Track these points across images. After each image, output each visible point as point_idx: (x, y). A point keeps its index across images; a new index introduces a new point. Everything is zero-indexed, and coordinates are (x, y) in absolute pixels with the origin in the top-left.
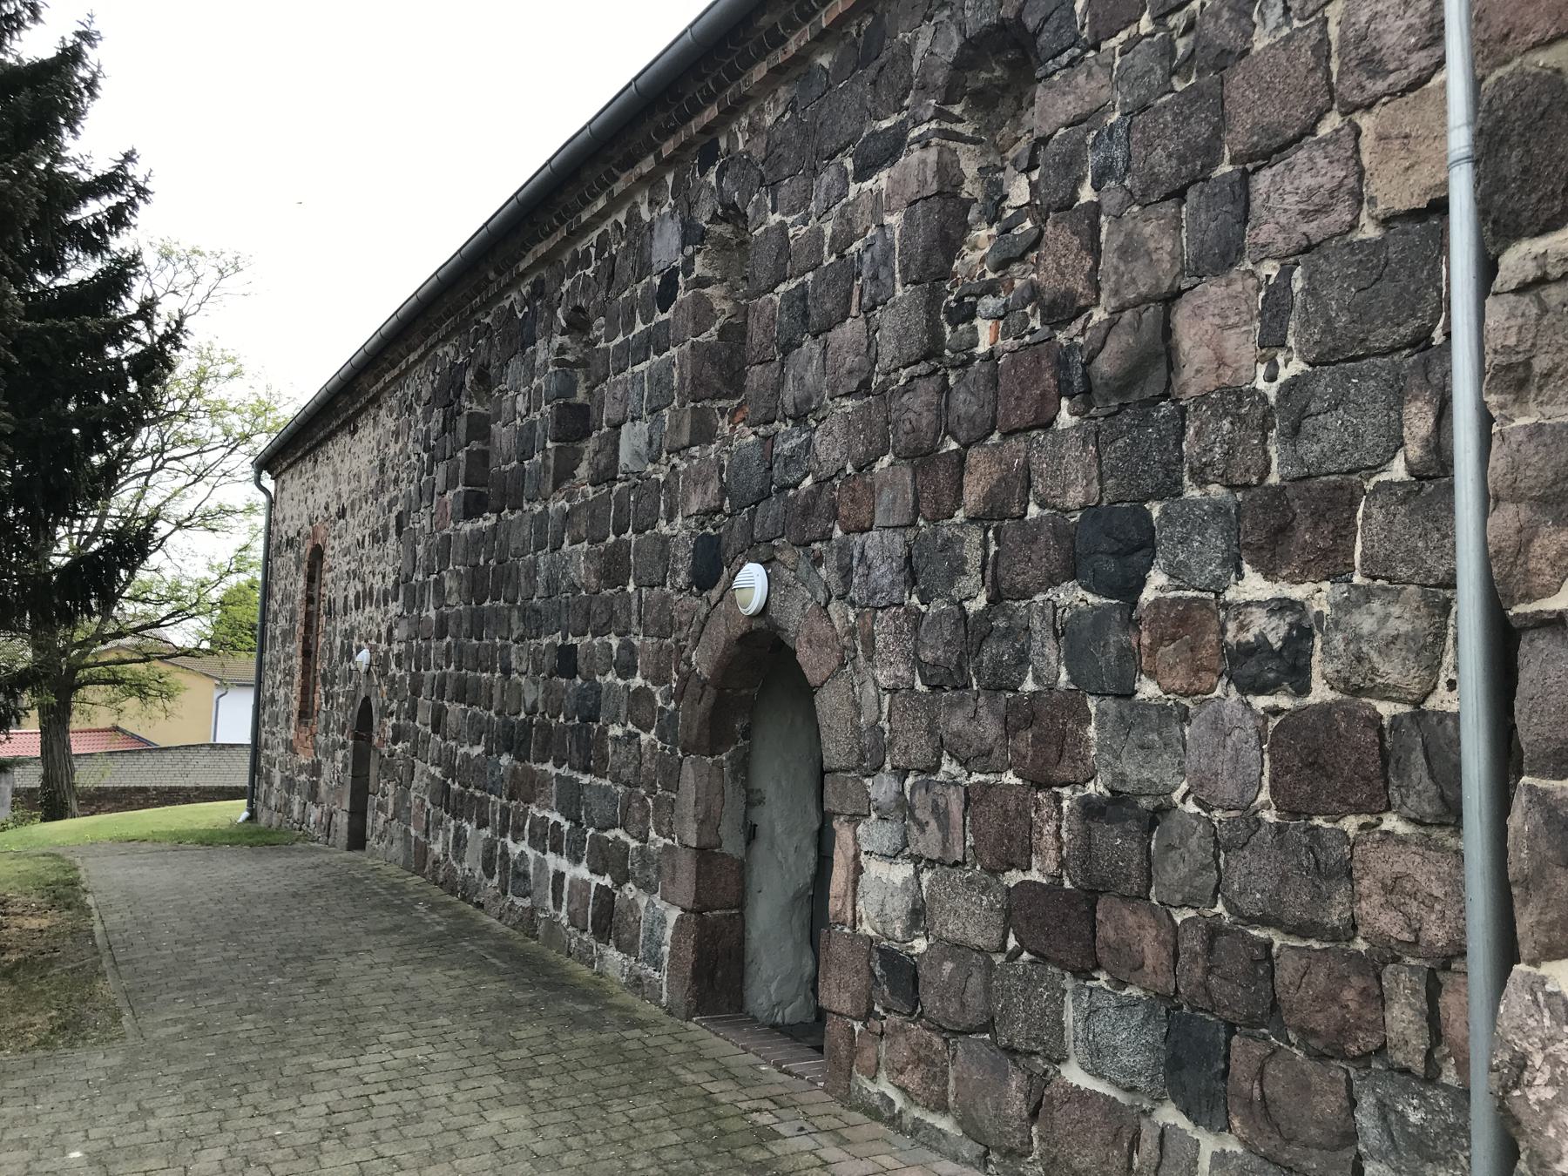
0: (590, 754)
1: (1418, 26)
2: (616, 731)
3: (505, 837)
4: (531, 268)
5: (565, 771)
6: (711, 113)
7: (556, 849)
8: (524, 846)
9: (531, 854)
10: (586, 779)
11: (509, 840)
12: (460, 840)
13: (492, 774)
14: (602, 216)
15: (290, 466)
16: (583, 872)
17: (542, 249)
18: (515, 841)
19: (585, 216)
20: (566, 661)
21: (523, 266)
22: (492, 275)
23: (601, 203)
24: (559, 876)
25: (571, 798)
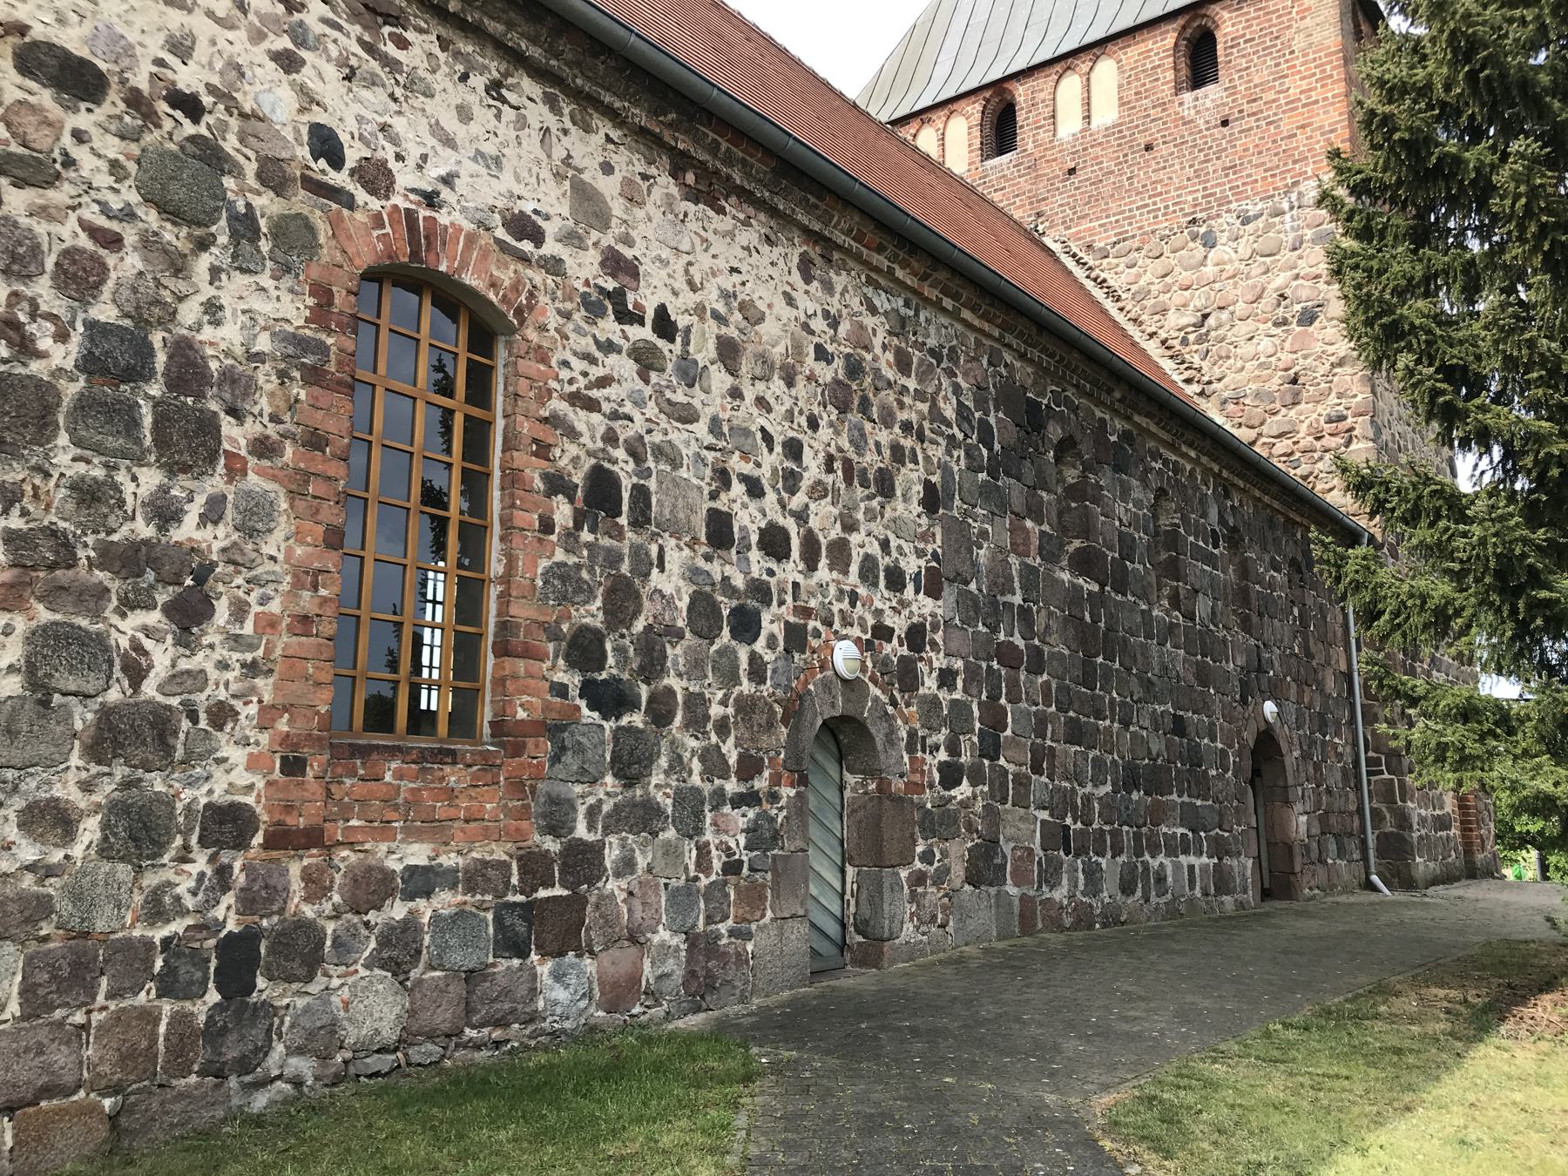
0: (1201, 786)
1: (208, 333)
2: (1214, 772)
3: (1023, 897)
4: (1138, 426)
5: (1185, 798)
6: (1241, 484)
7: (1186, 852)
8: (1161, 858)
9: (1167, 862)
10: (1199, 803)
11: (1147, 857)
12: (1093, 873)
13: (1127, 808)
14: (1185, 456)
15: (641, 133)
16: (1205, 859)
17: (1153, 428)
18: (1153, 857)
19: (1184, 449)
20: (1179, 727)
21: (1137, 418)
22: (1117, 395)
23: (1193, 454)
24: (1191, 868)
25: (1192, 819)
